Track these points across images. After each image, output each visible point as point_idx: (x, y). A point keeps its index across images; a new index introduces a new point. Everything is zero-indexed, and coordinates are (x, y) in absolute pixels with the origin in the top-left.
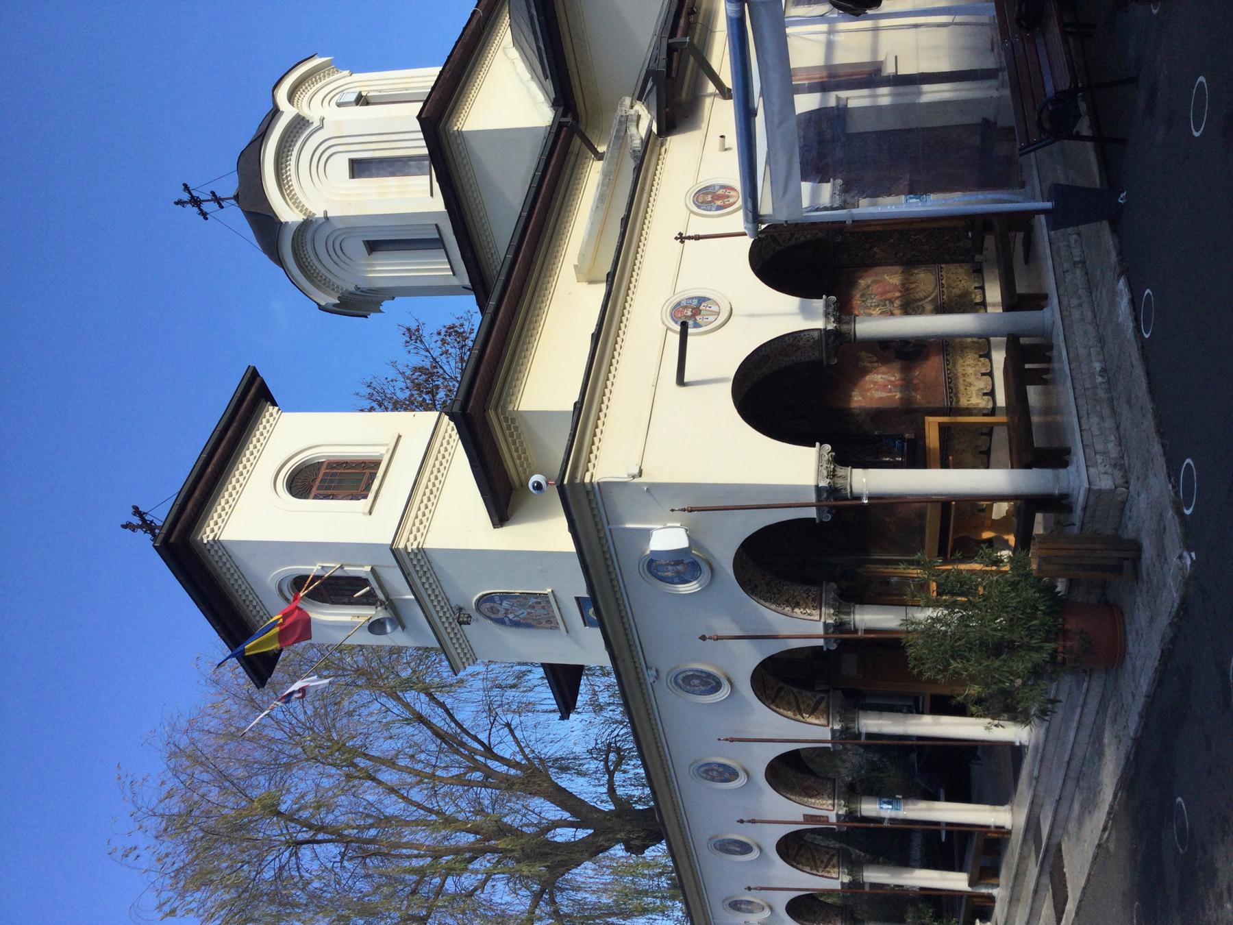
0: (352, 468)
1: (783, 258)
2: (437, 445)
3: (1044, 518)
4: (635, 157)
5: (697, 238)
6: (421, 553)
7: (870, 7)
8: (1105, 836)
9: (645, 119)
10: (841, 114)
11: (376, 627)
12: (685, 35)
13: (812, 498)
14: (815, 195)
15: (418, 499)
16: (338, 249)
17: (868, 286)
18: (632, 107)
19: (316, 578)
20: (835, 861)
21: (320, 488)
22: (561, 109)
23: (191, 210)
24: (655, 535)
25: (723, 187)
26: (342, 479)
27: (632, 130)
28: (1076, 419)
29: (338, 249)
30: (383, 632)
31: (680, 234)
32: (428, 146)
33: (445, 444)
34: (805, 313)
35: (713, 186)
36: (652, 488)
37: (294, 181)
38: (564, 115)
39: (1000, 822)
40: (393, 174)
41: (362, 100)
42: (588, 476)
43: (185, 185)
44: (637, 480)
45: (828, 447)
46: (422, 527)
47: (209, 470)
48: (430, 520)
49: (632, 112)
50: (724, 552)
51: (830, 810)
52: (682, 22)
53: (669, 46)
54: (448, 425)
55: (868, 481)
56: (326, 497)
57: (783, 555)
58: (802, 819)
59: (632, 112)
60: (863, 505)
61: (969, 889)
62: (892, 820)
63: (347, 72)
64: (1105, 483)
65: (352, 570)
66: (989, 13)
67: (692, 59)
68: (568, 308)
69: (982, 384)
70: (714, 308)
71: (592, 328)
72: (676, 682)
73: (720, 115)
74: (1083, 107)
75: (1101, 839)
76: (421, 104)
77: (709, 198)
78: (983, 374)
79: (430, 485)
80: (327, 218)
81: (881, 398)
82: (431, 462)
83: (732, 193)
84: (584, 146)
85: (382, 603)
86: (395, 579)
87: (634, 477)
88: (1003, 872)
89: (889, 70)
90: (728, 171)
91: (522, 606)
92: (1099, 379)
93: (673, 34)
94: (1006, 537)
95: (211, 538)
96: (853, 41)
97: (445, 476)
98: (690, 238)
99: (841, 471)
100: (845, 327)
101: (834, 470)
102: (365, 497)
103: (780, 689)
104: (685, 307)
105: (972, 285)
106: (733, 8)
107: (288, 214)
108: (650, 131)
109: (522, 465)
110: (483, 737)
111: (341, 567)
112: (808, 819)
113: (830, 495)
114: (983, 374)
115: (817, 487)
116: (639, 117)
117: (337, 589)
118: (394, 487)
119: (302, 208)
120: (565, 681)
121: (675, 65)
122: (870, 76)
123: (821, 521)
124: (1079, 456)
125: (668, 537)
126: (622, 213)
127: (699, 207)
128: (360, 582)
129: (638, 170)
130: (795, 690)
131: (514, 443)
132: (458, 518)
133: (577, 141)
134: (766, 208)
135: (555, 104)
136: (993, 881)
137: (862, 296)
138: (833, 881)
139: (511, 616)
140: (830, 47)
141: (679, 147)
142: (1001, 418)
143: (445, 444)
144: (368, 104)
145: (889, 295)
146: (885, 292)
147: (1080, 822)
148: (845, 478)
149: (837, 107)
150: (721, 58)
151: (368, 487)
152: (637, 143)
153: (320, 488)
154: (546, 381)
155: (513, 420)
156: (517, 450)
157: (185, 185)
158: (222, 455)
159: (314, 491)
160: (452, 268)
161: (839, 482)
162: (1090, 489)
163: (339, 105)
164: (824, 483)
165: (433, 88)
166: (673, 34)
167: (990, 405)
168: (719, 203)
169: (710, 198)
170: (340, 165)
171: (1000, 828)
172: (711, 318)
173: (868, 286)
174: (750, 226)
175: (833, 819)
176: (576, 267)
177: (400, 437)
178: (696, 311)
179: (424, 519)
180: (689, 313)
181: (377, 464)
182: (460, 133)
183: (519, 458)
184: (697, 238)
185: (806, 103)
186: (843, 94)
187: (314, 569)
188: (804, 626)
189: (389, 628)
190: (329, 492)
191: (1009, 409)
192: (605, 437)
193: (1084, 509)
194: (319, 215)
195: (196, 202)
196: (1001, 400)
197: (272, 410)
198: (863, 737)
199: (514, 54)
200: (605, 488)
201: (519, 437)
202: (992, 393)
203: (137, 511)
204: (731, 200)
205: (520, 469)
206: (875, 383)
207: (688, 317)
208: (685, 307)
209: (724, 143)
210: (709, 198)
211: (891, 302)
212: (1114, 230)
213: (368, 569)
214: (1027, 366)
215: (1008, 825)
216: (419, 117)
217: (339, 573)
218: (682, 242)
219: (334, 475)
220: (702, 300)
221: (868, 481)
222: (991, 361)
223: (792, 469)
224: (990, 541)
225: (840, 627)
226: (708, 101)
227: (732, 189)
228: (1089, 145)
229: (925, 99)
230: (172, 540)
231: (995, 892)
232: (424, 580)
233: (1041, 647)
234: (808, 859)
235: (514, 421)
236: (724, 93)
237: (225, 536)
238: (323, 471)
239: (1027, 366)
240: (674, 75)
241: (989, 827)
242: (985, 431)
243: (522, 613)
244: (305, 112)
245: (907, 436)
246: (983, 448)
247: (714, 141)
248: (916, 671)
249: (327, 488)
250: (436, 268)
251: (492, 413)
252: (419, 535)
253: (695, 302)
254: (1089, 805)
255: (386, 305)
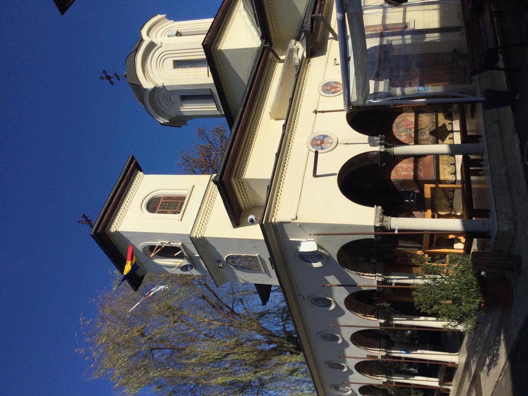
0: (173, 200)
1: (362, 118)
2: (209, 191)
3: (478, 241)
4: (297, 68)
5: (323, 112)
6: (203, 239)
7: (403, 3)
8: (501, 378)
9: (300, 50)
10: (390, 46)
11: (184, 268)
12: (319, 13)
13: (373, 231)
14: (376, 86)
15: (201, 215)
16: (168, 98)
17: (400, 122)
18: (295, 44)
19: (159, 247)
20: (380, 372)
21: (160, 208)
22: (264, 40)
23: (106, 81)
24: (303, 244)
25: (335, 83)
26: (170, 205)
27: (295, 55)
28: (493, 197)
29: (168, 98)
30: (187, 270)
31: (315, 110)
32: (206, 54)
33: (213, 190)
34: (372, 143)
35: (331, 82)
36: (301, 225)
37: (149, 69)
38: (266, 43)
39: (453, 361)
40: (192, 67)
41: (178, 34)
42: (273, 219)
43: (104, 71)
44: (295, 221)
45: (380, 207)
46: (203, 227)
47: (114, 200)
48: (206, 224)
49: (295, 47)
50: (333, 250)
51: (379, 353)
52: (318, 6)
53: (312, 17)
54: (214, 188)
55: (398, 223)
56: (163, 212)
57: (359, 252)
58: (366, 357)
59: (295, 47)
60: (395, 235)
61: (439, 386)
62: (406, 358)
63: (172, 21)
64: (506, 228)
65: (173, 244)
66: (459, 2)
67: (322, 23)
68: (267, 132)
69: (450, 169)
70: (330, 141)
71: (276, 151)
72: (312, 303)
73: (333, 47)
74: (501, 57)
75: (498, 379)
76: (205, 35)
77: (329, 88)
78: (451, 164)
79: (206, 208)
80: (164, 86)
81: (405, 175)
82: (207, 198)
83: (339, 86)
84: (274, 57)
85: (186, 258)
86: (192, 248)
87: (294, 220)
88: (454, 380)
89: (411, 27)
90: (337, 76)
91: (246, 261)
92: (504, 178)
93: (314, 12)
94: (459, 238)
95: (114, 230)
96: (395, 16)
97: (213, 204)
98: (319, 112)
99: (386, 218)
100: (389, 150)
101: (383, 218)
102: (179, 213)
103: (358, 304)
104: (317, 140)
105: (447, 122)
106: (340, 15)
107: (147, 85)
108: (303, 57)
109: (246, 201)
110: (231, 306)
111: (169, 243)
112: (368, 356)
113: (380, 229)
114: (451, 164)
115: (375, 226)
116: (298, 49)
117: (168, 252)
118: (191, 209)
119: (153, 82)
120: (264, 291)
121: (314, 26)
122: (403, 30)
123: (377, 240)
124: (493, 213)
125: (308, 246)
126: (290, 96)
127: (324, 92)
128: (177, 249)
129: (297, 75)
130: (364, 305)
131: (243, 192)
132: (218, 224)
133: (271, 54)
134: (354, 97)
135: (262, 38)
136: (450, 383)
137: (397, 127)
138: (380, 380)
139: (241, 265)
140: (384, 18)
141: (315, 61)
142: (460, 186)
143: (213, 190)
144: (181, 35)
145: (409, 127)
146: (408, 125)
147: (489, 369)
148: (387, 222)
149: (387, 44)
150: (334, 24)
151: (180, 209)
152: (297, 62)
153: (160, 208)
154: (258, 165)
155: (242, 183)
156: (244, 195)
157: (104, 71)
158: (119, 194)
159: (158, 210)
160: (217, 107)
161: (385, 224)
162: (499, 231)
163: (169, 36)
164: (378, 225)
165: (209, 31)
166: (314, 12)
167: (454, 179)
168: (333, 90)
169: (328, 88)
170: (169, 63)
171: (453, 363)
172: (329, 145)
173: (400, 122)
174: (347, 108)
175: (380, 357)
176: (270, 113)
177: (194, 186)
178: (322, 142)
179: (204, 224)
180: (319, 143)
181: (184, 198)
182: (221, 51)
183: (245, 198)
184: (323, 112)
185: (372, 43)
186: (390, 38)
187: (158, 243)
188: (369, 281)
189: (189, 269)
190: (164, 210)
191: (462, 181)
192: (283, 189)
193: (496, 239)
194: (160, 85)
195: (109, 78)
196: (459, 177)
197: (140, 173)
198: (394, 326)
199: (244, 13)
200: (282, 224)
201: (245, 189)
202: (455, 174)
203: (84, 216)
204: (339, 89)
205: (245, 203)
206: (402, 168)
207: (319, 143)
208: (317, 140)
209: (336, 62)
210: (329, 88)
211: (410, 130)
212: (513, 110)
213: (180, 244)
214: (471, 168)
215: (457, 362)
216: (203, 44)
217: (169, 245)
218: (316, 113)
219: (166, 202)
220: (325, 136)
221: (398, 223)
222: (455, 158)
223: (365, 217)
224: (452, 239)
225: (384, 282)
226: (329, 41)
227: (339, 83)
228: (503, 72)
229: (427, 40)
230: (98, 232)
231: (450, 388)
232: (204, 249)
233: (475, 302)
234: (368, 371)
235: (243, 183)
236: (335, 38)
237: (120, 230)
238: (161, 201)
239: (471, 168)
240: (314, 31)
241: (448, 362)
242: (451, 190)
243: (246, 264)
244: (155, 41)
245: (416, 191)
246: (451, 197)
247: (331, 61)
248: (417, 308)
249: (164, 208)
250: (210, 108)
251: (233, 180)
252: (202, 231)
253: (322, 137)
254: (493, 363)
255: (189, 122)
